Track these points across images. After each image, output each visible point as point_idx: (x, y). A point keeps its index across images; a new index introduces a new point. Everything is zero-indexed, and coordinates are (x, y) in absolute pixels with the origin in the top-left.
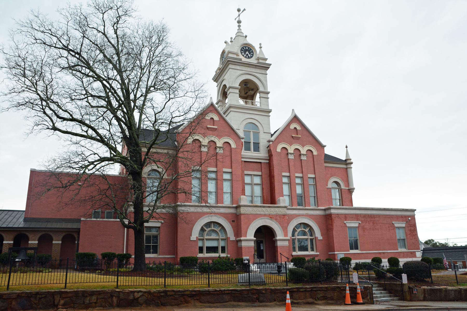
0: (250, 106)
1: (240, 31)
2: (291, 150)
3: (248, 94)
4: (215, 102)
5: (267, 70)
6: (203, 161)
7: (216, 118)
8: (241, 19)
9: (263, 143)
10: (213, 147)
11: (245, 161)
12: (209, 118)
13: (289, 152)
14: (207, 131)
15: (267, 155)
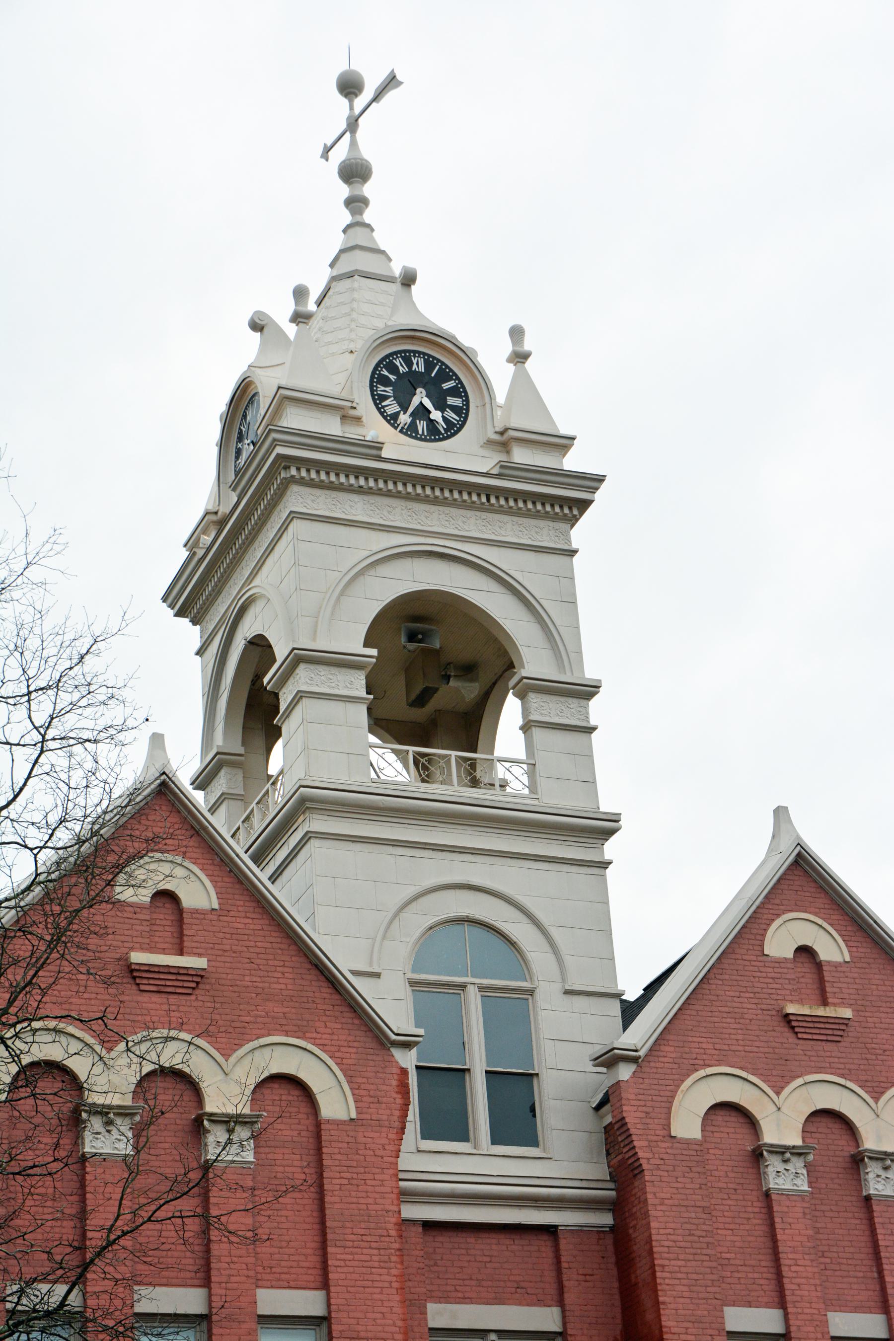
0: (450, 790)
1: (359, 237)
2: (781, 1125)
3: (434, 703)
4: (185, 766)
5: (573, 521)
6: (95, 1239)
7: (197, 892)
8: (368, 152)
9: (564, 1074)
10: (178, 1118)
11: (429, 1226)
12: (145, 896)
13: (770, 1136)
14: (130, 994)
15: (600, 1171)
